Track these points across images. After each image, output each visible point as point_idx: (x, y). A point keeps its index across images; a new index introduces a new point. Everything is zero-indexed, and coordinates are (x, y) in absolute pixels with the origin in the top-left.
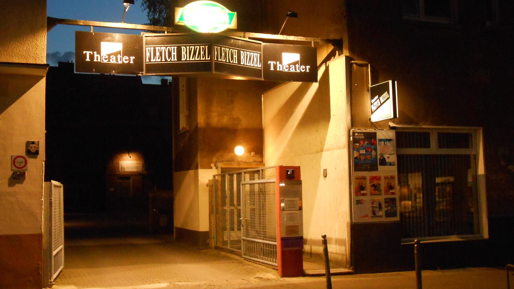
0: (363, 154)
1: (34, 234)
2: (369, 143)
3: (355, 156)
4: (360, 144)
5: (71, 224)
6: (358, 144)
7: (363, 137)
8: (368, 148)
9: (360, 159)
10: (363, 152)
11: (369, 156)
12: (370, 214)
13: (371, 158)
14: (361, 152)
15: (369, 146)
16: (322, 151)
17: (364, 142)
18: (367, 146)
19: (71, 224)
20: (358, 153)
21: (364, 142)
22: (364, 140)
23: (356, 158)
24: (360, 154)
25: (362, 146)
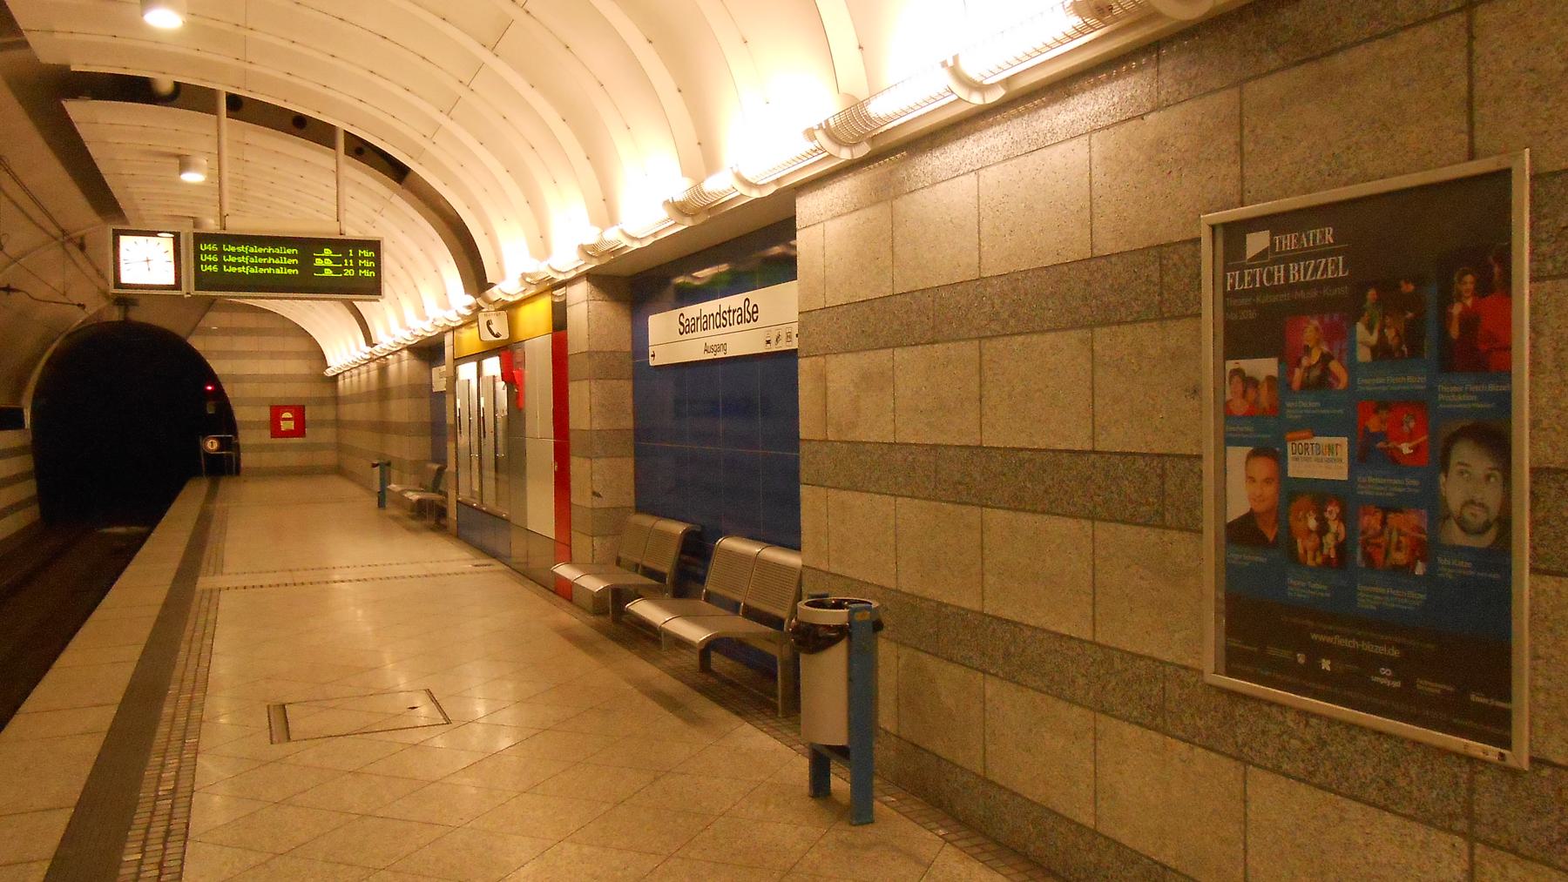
0: (1320, 494)
1: (1509, 653)
2: (1413, 337)
3: (1238, 507)
4: (1289, 360)
5: (1235, 644)
6: (1264, 367)
7: (1334, 268)
8: (1382, 404)
9: (1287, 543)
10: (1323, 460)
11: (1410, 521)
12: (1176, 334)
13: (1423, 549)
14: (1301, 467)
15: (1413, 380)
16: (1470, 837)
17: (1337, 333)
18: (1371, 384)
19: (1235, 644)
20: (1262, 468)
21: (1337, 333)
22: (1338, 309)
23: (1243, 532)
24: (1293, 492)
25: (1321, 382)
